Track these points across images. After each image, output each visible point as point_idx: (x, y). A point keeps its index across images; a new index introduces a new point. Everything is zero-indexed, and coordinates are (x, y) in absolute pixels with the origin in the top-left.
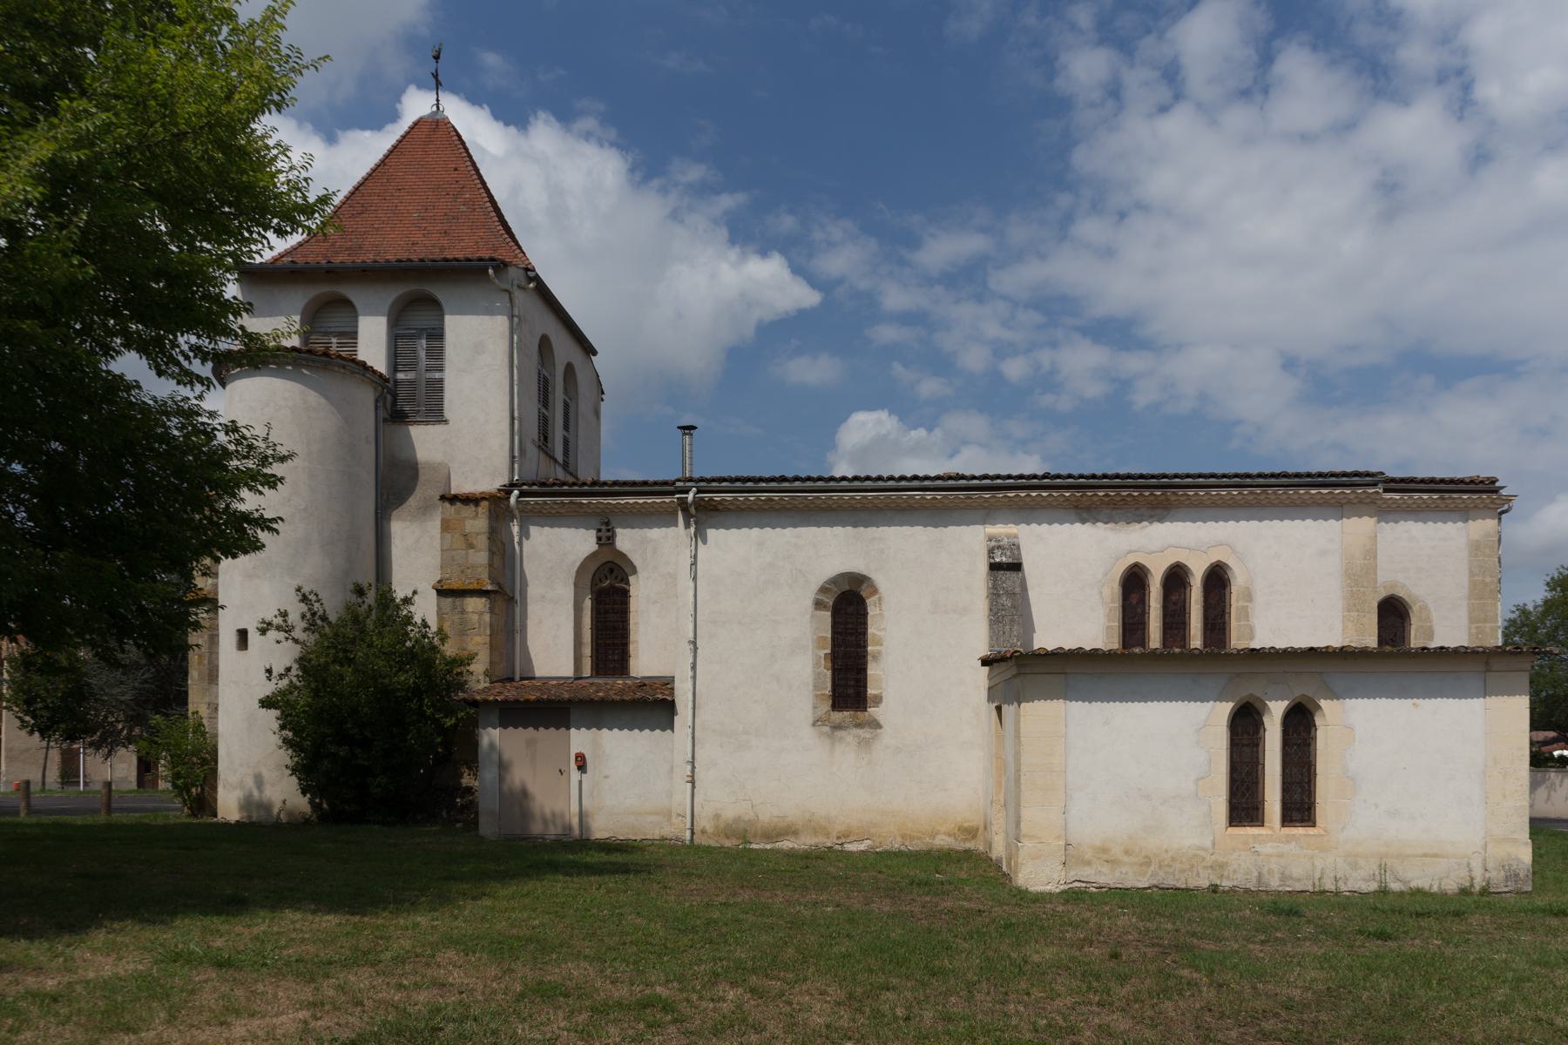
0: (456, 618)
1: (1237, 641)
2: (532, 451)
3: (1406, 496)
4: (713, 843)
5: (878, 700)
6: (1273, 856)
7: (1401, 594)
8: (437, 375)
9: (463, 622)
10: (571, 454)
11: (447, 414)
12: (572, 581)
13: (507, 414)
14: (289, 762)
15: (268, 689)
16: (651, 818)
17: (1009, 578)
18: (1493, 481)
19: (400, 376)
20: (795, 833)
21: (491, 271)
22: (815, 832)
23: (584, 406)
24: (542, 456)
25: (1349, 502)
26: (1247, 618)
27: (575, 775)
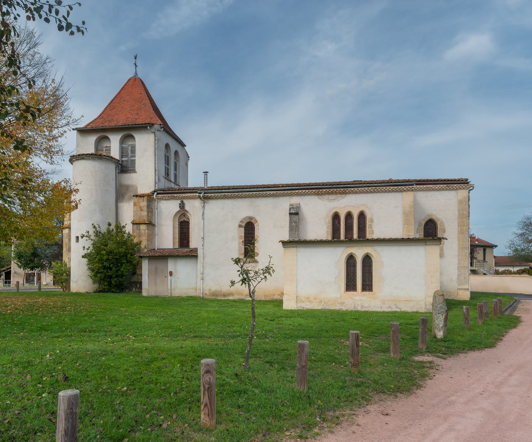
0: (138, 231)
1: (369, 236)
2: (163, 180)
3: (435, 186)
4: (208, 298)
5: (258, 254)
6: (359, 301)
7: (434, 218)
8: (134, 158)
9: (139, 233)
10: (177, 180)
11: (136, 170)
12: (172, 219)
13: (154, 169)
14: (90, 274)
15: (86, 251)
16: (191, 290)
17: (295, 218)
18: (467, 180)
19: (124, 159)
20: (233, 295)
21: (148, 127)
22: (239, 294)
23: (181, 163)
24: (166, 180)
25: (405, 191)
26: (371, 228)
27: (169, 277)
